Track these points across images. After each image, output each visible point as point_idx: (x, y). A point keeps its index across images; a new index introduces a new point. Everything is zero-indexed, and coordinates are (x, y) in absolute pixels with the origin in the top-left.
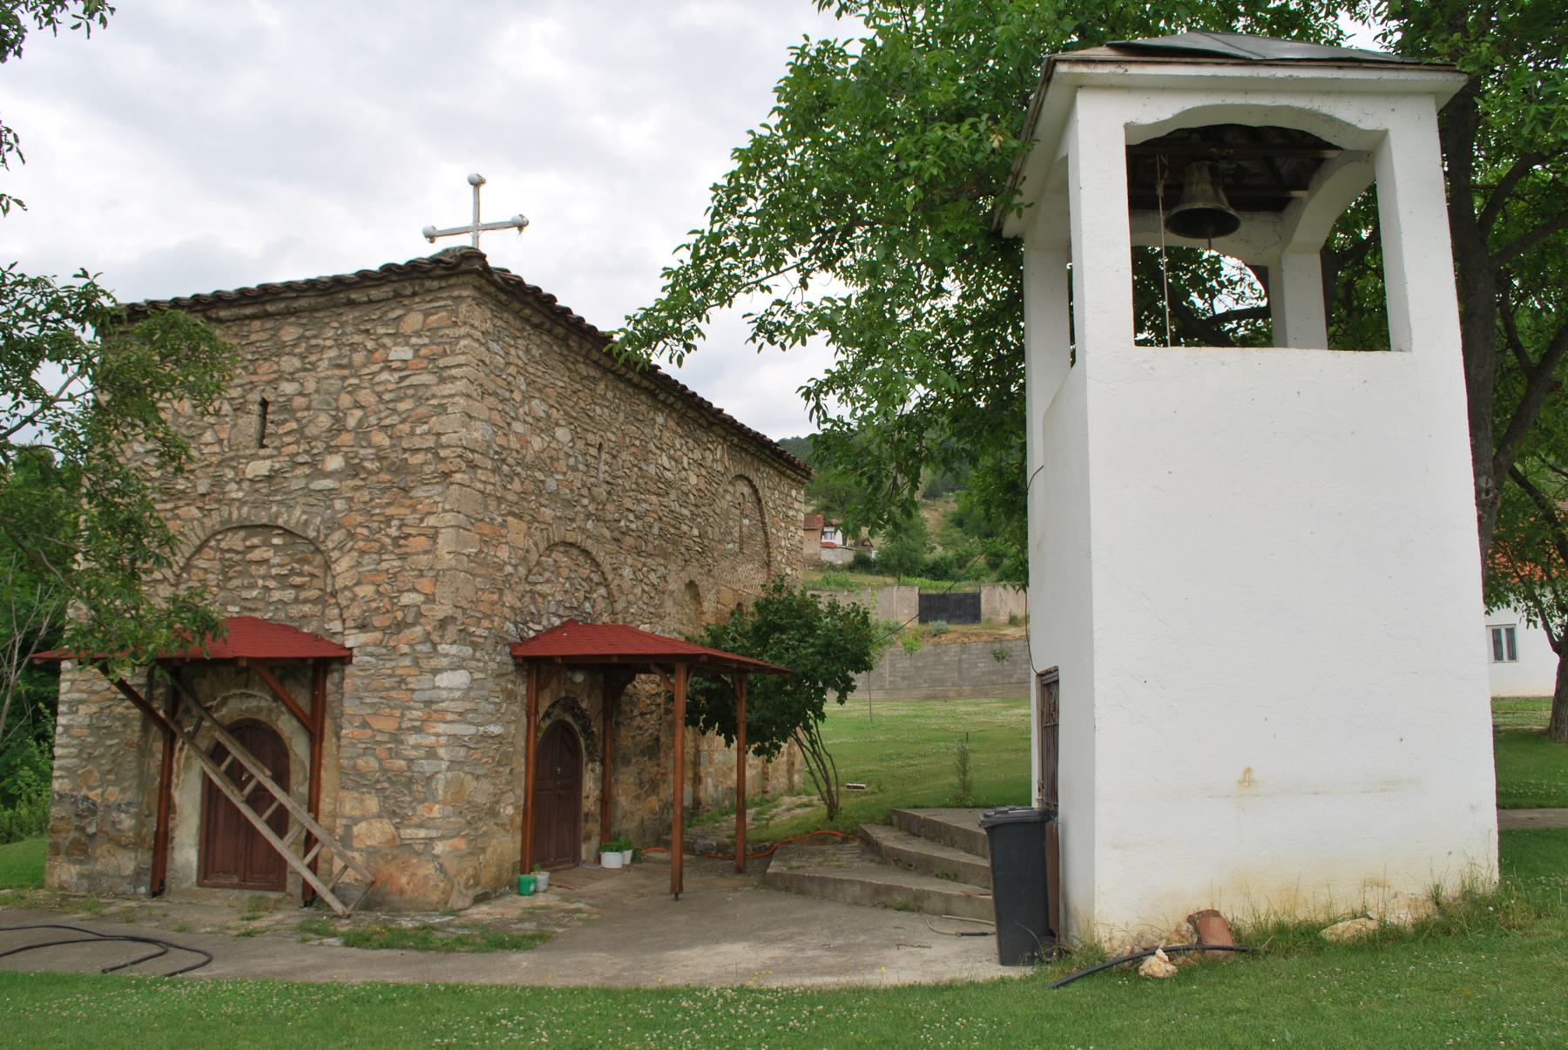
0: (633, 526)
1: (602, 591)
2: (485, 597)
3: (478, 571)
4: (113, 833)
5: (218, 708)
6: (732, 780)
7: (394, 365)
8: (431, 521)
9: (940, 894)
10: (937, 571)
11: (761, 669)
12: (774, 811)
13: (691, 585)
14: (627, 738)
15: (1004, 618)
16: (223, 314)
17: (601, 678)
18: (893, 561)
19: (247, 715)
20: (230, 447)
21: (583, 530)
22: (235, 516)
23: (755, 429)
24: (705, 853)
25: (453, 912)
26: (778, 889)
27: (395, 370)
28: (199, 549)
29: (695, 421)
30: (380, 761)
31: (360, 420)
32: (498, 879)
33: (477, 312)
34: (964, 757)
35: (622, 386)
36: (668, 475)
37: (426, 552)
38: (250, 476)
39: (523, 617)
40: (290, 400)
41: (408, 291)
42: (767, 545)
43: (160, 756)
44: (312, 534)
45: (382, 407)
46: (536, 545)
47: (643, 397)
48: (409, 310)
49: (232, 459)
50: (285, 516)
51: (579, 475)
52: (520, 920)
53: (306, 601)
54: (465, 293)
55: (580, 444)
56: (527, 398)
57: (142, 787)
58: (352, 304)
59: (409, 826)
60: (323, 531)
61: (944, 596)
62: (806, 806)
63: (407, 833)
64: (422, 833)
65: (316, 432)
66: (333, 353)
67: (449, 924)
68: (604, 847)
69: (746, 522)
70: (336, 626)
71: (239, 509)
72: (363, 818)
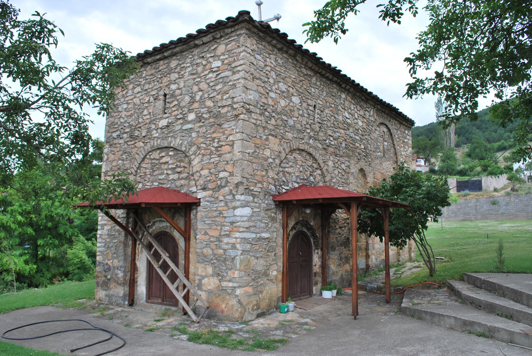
0: (333, 143)
1: (319, 172)
2: (259, 173)
3: (254, 161)
4: (116, 279)
5: (151, 227)
6: (383, 257)
7: (214, 70)
8: (231, 138)
9: (506, 330)
10: (462, 173)
11: (395, 205)
12: (403, 270)
13: (362, 170)
14: (333, 239)
15: (492, 189)
16: (149, 60)
17: (320, 211)
18: (445, 170)
19: (162, 230)
20: (153, 115)
21: (308, 144)
22: (155, 144)
23: (387, 102)
24: (371, 291)
25: (246, 323)
26: (408, 316)
27: (214, 72)
28: (143, 160)
29: (360, 98)
30: (212, 250)
31: (201, 96)
32: (269, 305)
33: (249, 41)
34: (501, 248)
35: (324, 80)
36: (348, 121)
37: (229, 153)
38: (160, 127)
39: (278, 183)
40: (174, 92)
41: (218, 36)
42: (396, 154)
43: (131, 247)
44: (183, 149)
45: (209, 89)
46: (284, 149)
47: (334, 85)
48: (219, 44)
49: (154, 120)
50: (174, 142)
51: (305, 119)
52: (276, 329)
53: (182, 179)
54: (242, 32)
55: (305, 105)
56: (276, 82)
57: (125, 260)
58: (196, 46)
59: (225, 281)
60: (188, 147)
61: (467, 181)
62: (418, 267)
63: (224, 284)
64: (231, 284)
65: (184, 104)
66: (189, 69)
67: (241, 330)
68: (323, 289)
69: (386, 143)
70: (194, 189)
71: (157, 141)
72: (206, 276)
